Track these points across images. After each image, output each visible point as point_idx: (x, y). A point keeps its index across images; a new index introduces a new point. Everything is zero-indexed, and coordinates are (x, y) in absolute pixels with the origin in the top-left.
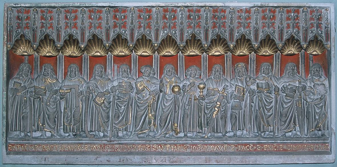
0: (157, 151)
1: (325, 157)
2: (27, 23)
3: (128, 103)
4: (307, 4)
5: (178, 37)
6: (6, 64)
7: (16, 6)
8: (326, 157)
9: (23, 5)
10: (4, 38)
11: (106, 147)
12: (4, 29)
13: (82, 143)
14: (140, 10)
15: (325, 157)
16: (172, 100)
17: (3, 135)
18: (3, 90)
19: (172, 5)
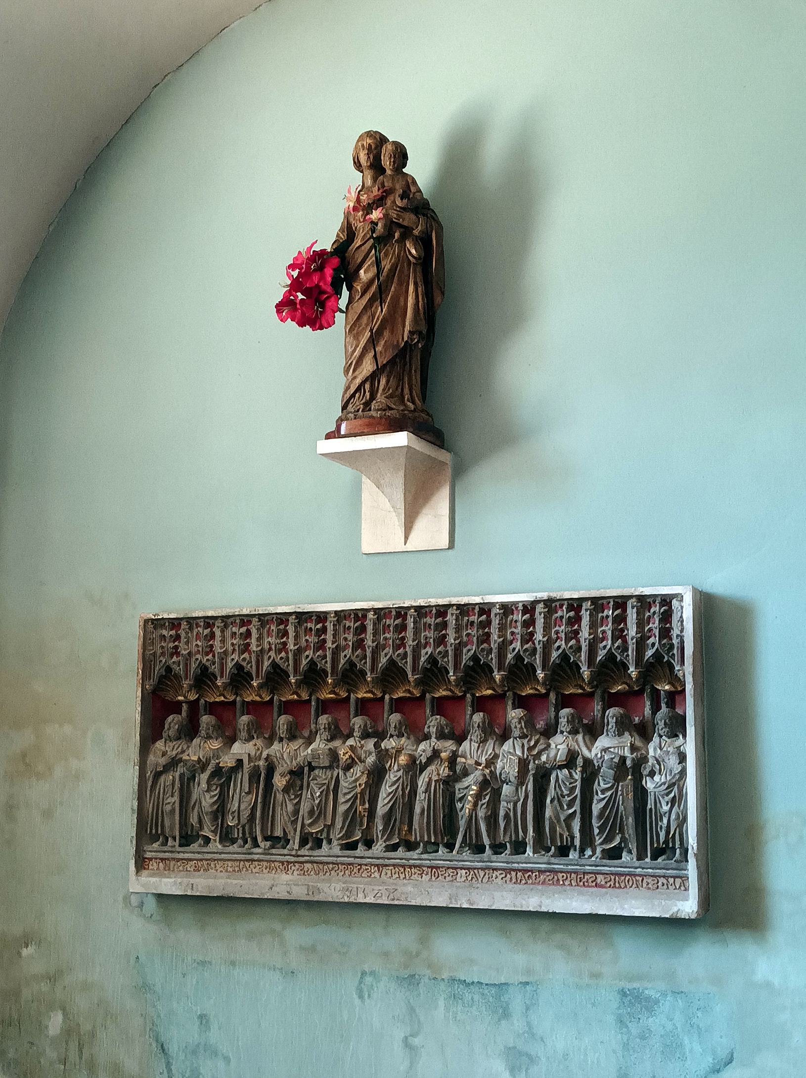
0: (669, 723)
1: (676, 906)
2: (176, 647)
3: (328, 787)
4: (635, 590)
5: (408, 664)
6: (139, 719)
7: (156, 617)
8: (678, 904)
9: (166, 616)
10: (138, 672)
11: (291, 867)
12: (139, 658)
13: (253, 860)
14: (341, 615)
15: (676, 906)
16: (397, 785)
17: (131, 841)
18: (135, 763)
19: (394, 606)
